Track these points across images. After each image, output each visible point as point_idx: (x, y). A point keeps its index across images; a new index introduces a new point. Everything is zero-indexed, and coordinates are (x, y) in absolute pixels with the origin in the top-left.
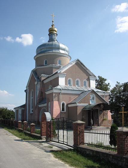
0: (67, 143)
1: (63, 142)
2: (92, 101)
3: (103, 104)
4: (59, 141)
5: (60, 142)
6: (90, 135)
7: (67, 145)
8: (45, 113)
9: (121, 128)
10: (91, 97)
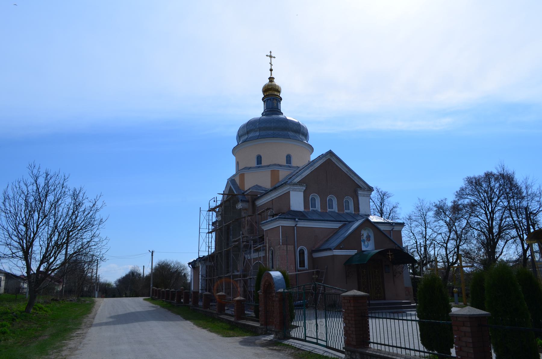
0: (326, 341)
1: (317, 339)
2: (366, 243)
3: (392, 250)
4: (306, 337)
5: (308, 339)
6: (385, 325)
7: (327, 347)
8: (540, 354)
9: (346, 235)
10: (363, 235)
